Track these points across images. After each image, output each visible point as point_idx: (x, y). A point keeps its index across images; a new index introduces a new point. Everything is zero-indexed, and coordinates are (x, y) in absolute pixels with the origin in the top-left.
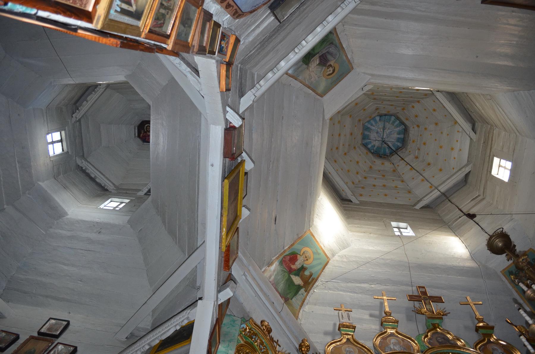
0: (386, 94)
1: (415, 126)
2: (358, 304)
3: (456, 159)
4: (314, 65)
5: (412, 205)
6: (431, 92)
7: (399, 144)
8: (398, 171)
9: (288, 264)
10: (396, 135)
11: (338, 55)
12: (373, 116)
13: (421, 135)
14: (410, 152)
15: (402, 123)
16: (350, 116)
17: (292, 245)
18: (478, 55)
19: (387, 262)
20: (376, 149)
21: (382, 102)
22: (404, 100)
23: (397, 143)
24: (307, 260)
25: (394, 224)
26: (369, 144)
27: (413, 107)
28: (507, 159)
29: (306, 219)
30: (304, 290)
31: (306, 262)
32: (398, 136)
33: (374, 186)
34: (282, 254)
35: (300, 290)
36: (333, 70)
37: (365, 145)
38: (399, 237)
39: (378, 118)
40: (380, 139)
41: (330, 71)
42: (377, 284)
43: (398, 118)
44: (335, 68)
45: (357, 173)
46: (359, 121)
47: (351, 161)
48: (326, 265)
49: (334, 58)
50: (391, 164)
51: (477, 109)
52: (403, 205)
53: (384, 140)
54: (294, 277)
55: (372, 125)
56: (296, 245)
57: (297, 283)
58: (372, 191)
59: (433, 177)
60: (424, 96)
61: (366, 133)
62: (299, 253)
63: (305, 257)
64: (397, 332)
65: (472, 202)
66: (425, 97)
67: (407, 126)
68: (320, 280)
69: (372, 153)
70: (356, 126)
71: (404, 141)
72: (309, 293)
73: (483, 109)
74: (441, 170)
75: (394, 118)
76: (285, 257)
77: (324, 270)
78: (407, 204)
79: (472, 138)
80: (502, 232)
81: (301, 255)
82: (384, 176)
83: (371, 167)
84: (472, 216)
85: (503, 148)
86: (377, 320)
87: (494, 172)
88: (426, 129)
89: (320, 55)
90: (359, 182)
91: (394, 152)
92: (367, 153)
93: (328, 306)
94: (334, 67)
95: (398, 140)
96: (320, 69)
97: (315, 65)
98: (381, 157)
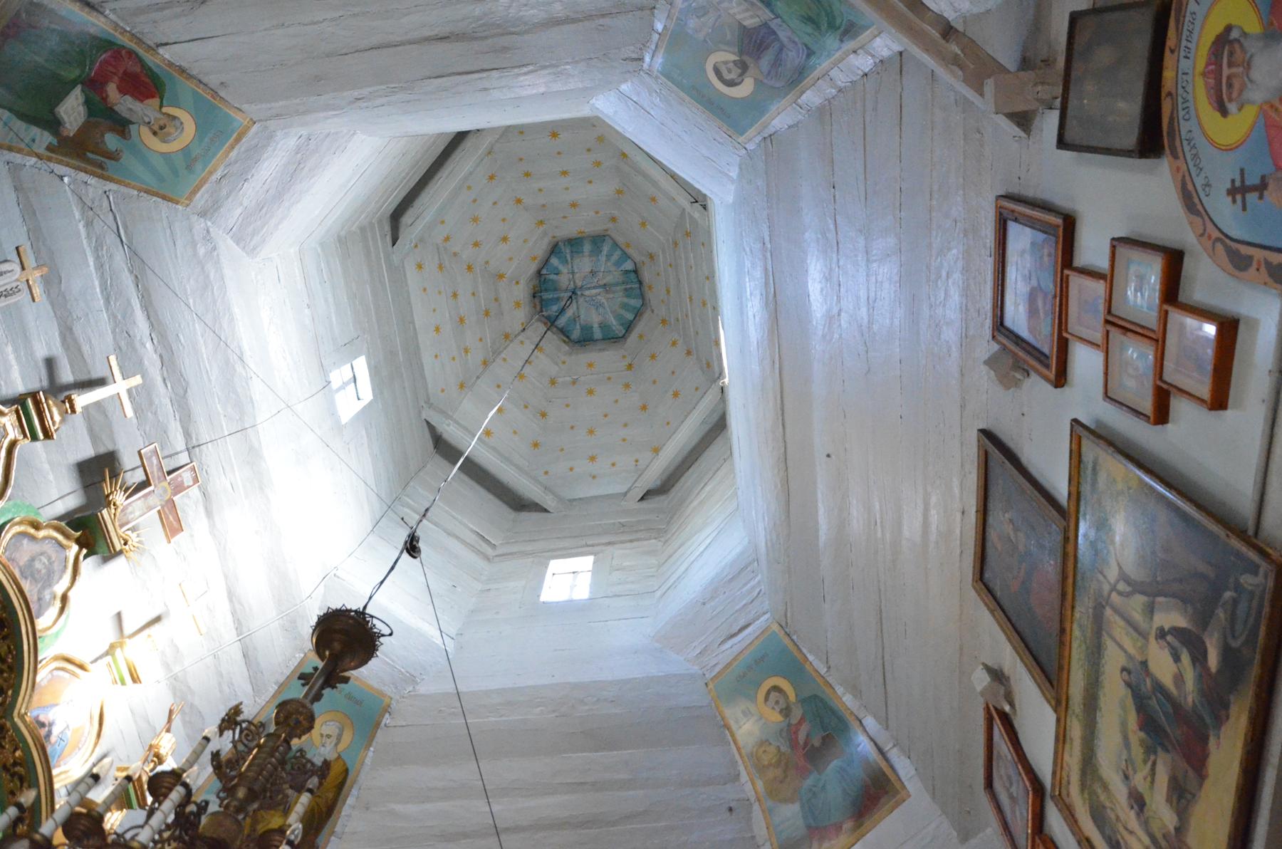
0: (693, 269)
1: (628, 360)
2: (75, 317)
3: (571, 473)
4: (739, 13)
5: (431, 401)
6: (717, 375)
7: (576, 334)
8: (508, 345)
9: (110, 68)
10: (596, 320)
11: (778, 85)
12: (631, 251)
13: (609, 379)
14: (564, 363)
15: (629, 327)
16: (619, 192)
17: (182, 71)
18: (833, 457)
19: (238, 369)
20: (552, 280)
21: (670, 265)
22: (687, 316)
23: (578, 327)
24: (155, 133)
25: (361, 364)
26: (559, 258)
27: (674, 344)
28: (595, 585)
29: (281, 103)
30: (50, 143)
31: (145, 131)
32: (596, 326)
33: (455, 295)
34: (140, 42)
35: (44, 129)
36: (733, 80)
37: (554, 249)
38: (325, 384)
39: (628, 266)
40: (579, 284)
41: (729, 71)
42: (161, 356)
43: (638, 314)
44: (740, 83)
45: (476, 244)
46: (613, 219)
47: (504, 220)
48: (164, 198)
49: (769, 72)
50: (522, 324)
51: (700, 488)
52: (423, 377)
53: (579, 293)
54: (77, 99)
55: (609, 256)
56: (191, 85)
57: (62, 114)
58: (440, 293)
59: (515, 433)
60: (704, 362)
61: (587, 247)
62: (164, 102)
63: (162, 123)
64: (13, 444)
65: (474, 536)
66: (705, 366)
67: (626, 339)
68: (106, 188)
69: (539, 273)
70: (597, 213)
71: (583, 340)
72: (50, 159)
73: (700, 502)
74: (536, 445)
75: (638, 306)
76: (134, 56)
77: (145, 195)
78: (430, 386)
79: (628, 495)
80: (379, 637)
81: (164, 110)
82: (487, 313)
83: (501, 276)
84: (412, 547)
85: (617, 570)
86: (41, 381)
87: (556, 565)
88: (627, 386)
89: (773, 25)
90: (455, 254)
91: (551, 322)
92: (534, 258)
93: (28, 231)
94: (743, 80)
95: (587, 329)
96: (729, 37)
97: (738, 17)
98: (534, 297)
